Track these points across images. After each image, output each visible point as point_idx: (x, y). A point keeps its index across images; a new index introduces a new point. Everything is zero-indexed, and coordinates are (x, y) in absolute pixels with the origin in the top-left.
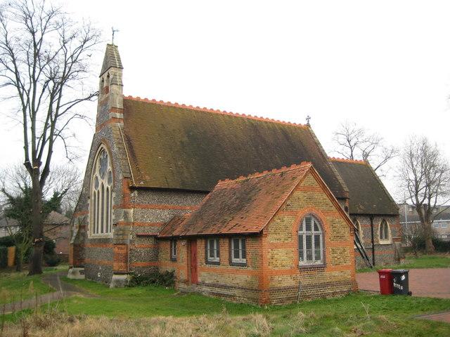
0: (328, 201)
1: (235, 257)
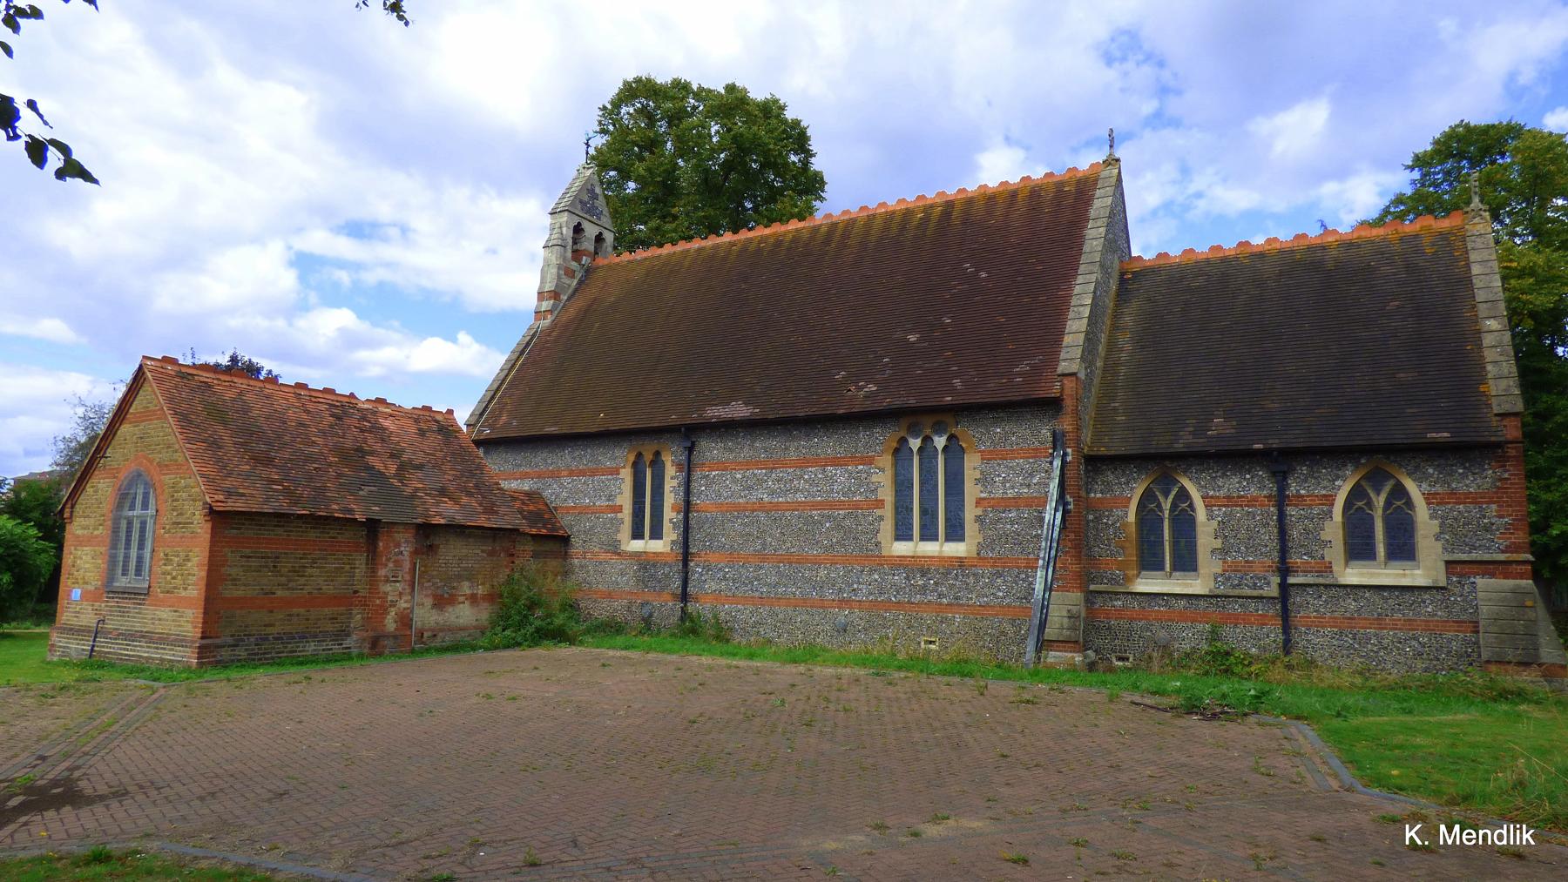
1: (898, 538)
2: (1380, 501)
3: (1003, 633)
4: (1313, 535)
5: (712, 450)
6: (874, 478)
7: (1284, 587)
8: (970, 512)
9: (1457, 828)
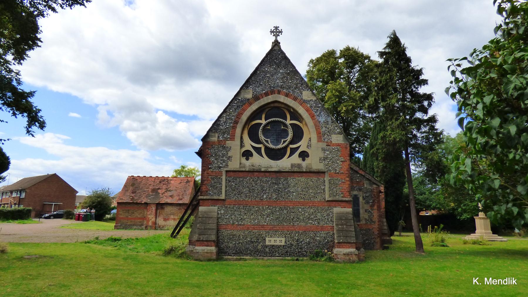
9: (491, 279)
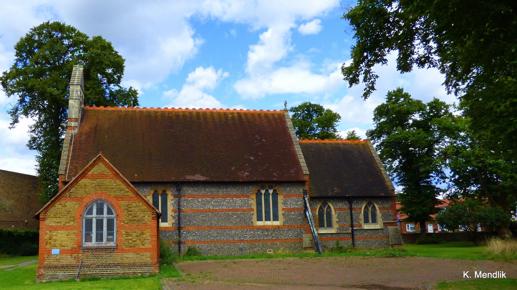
0: (123, 186)
1: (258, 220)
2: (370, 209)
3: (291, 247)
4: (358, 217)
5: (188, 191)
6: (250, 202)
7: (353, 230)
8: (280, 212)
9: (480, 272)
